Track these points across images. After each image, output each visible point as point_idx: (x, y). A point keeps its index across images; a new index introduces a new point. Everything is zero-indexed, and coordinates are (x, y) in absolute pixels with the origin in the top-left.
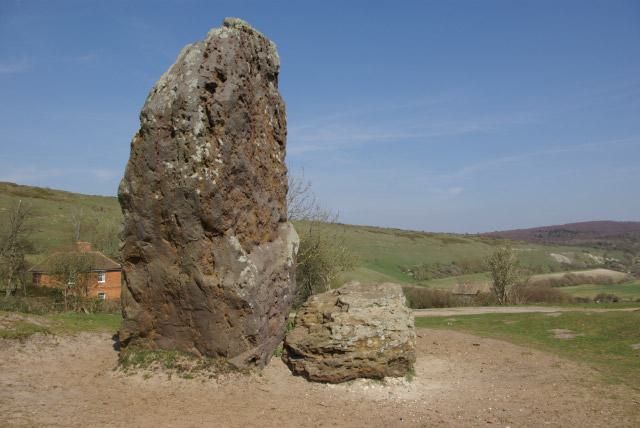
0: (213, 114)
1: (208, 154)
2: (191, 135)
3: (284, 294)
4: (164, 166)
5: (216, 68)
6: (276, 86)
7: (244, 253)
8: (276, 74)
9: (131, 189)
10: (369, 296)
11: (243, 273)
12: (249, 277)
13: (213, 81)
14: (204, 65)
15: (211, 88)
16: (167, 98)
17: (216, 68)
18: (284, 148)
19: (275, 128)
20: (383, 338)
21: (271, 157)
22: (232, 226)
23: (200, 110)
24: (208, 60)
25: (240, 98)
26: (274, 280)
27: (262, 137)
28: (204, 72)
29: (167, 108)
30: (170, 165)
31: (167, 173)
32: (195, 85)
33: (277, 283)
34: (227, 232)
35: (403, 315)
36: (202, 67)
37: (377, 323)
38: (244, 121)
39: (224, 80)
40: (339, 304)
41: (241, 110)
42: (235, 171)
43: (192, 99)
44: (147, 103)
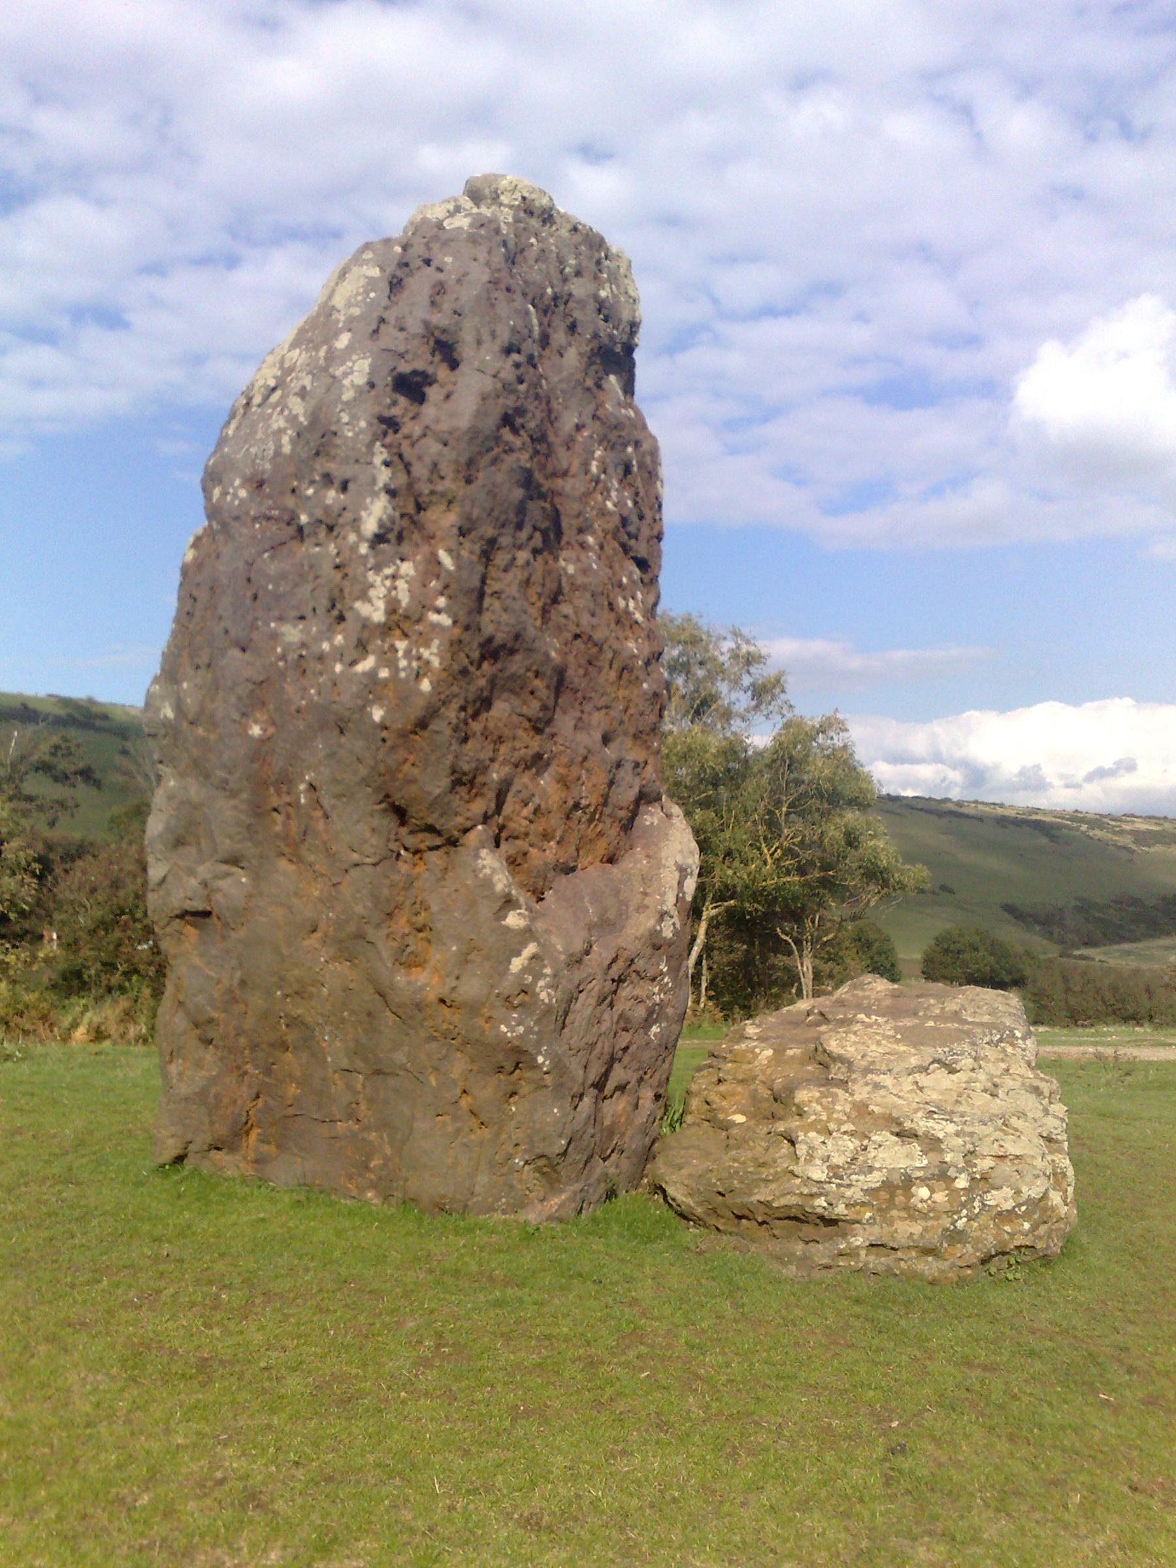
0: (420, 470)
1: (404, 599)
2: (352, 537)
3: (648, 1022)
4: (275, 636)
5: (426, 324)
6: (629, 388)
7: (523, 898)
8: (629, 349)
9: (179, 707)
10: (914, 1038)
11: (517, 964)
12: (538, 976)
13: (419, 365)
14: (391, 316)
15: (412, 387)
16: (278, 422)
17: (426, 324)
18: (654, 581)
19: (624, 521)
20: (962, 1182)
21: (611, 607)
22: (486, 819)
23: (378, 460)
24: (404, 296)
25: (507, 420)
26: (619, 981)
27: (583, 546)
28: (391, 337)
29: (278, 453)
30: (292, 633)
31: (283, 657)
32: (360, 379)
33: (626, 991)
34: (472, 837)
35: (1030, 1103)
36: (382, 320)
37: (942, 1129)
38: (519, 493)
39: (454, 364)
40: (823, 1060)
41: (510, 460)
42: (491, 651)
43: (354, 427)
44: (222, 441)
